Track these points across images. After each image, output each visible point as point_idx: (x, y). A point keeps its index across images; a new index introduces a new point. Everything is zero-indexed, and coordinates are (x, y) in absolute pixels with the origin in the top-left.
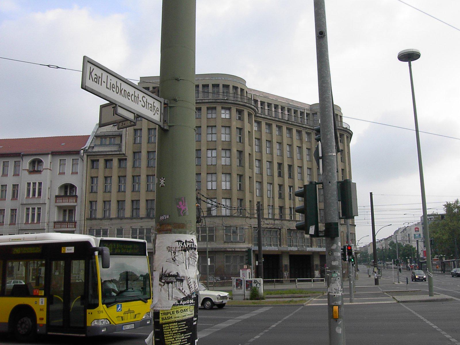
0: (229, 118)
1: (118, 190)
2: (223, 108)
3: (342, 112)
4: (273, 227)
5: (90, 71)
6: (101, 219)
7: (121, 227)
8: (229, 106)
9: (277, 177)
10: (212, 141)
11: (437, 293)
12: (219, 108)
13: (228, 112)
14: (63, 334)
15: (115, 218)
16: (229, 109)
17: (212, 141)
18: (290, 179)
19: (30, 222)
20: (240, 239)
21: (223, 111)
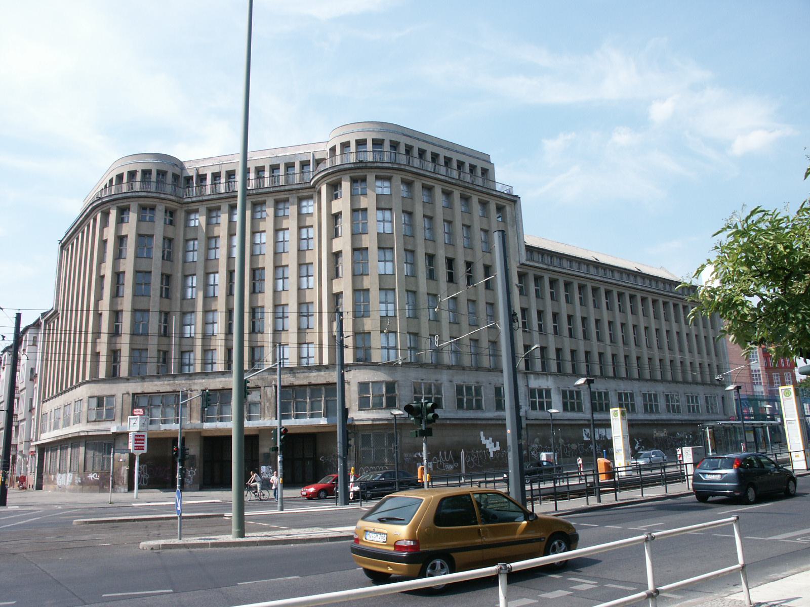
0: (389, 193)
1: (120, 316)
2: (378, 178)
3: (492, 162)
4: (171, 390)
5: (757, 209)
6: (489, 370)
7: (478, 383)
8: (389, 174)
9: (484, 289)
10: (384, 233)
11: (787, 541)
12: (371, 178)
13: (387, 184)
14: (119, 594)
15: (470, 368)
16: (389, 179)
17: (384, 233)
18: (522, 297)
19: (102, 375)
20: (107, 415)
21: (379, 183)
